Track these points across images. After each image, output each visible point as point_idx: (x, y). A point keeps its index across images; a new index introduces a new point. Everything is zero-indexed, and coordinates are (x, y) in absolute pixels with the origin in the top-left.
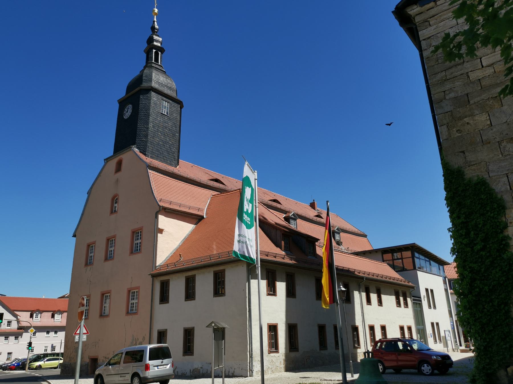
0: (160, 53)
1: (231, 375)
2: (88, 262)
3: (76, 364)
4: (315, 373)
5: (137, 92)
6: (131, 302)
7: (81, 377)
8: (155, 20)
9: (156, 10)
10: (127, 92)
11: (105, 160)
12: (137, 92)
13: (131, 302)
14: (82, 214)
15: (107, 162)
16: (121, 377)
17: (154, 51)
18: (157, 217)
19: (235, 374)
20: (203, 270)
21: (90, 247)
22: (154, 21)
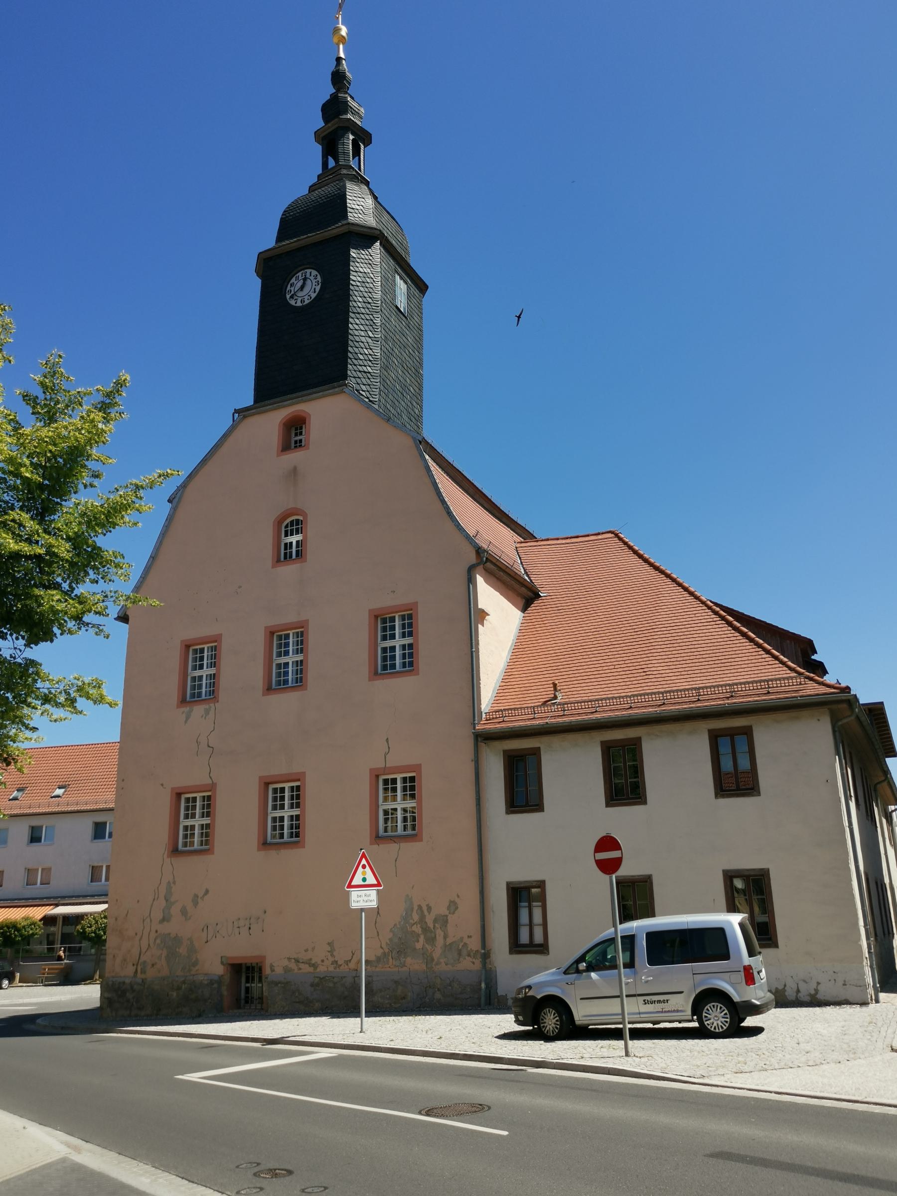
0: (362, 146)
1: (803, 996)
2: (193, 694)
3: (360, 977)
4: (256, 1023)
5: (316, 237)
6: (184, 822)
7: (369, 1014)
8: (342, 55)
9: (344, 31)
10: (282, 235)
11: (236, 411)
12: (316, 237)
13: (184, 822)
14: (153, 558)
15: (245, 417)
16: (645, 1002)
17: (351, 137)
18: (471, 581)
19: (820, 997)
20: (571, 737)
21: (199, 652)
22: (339, 59)
